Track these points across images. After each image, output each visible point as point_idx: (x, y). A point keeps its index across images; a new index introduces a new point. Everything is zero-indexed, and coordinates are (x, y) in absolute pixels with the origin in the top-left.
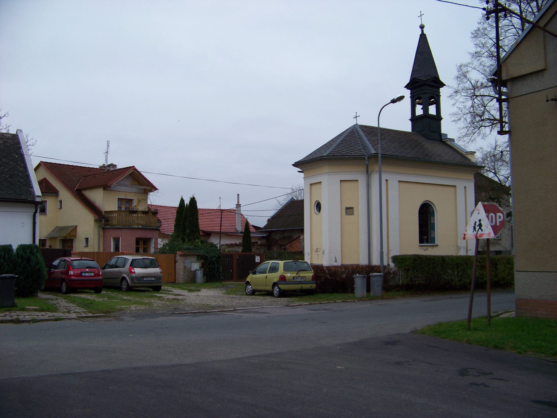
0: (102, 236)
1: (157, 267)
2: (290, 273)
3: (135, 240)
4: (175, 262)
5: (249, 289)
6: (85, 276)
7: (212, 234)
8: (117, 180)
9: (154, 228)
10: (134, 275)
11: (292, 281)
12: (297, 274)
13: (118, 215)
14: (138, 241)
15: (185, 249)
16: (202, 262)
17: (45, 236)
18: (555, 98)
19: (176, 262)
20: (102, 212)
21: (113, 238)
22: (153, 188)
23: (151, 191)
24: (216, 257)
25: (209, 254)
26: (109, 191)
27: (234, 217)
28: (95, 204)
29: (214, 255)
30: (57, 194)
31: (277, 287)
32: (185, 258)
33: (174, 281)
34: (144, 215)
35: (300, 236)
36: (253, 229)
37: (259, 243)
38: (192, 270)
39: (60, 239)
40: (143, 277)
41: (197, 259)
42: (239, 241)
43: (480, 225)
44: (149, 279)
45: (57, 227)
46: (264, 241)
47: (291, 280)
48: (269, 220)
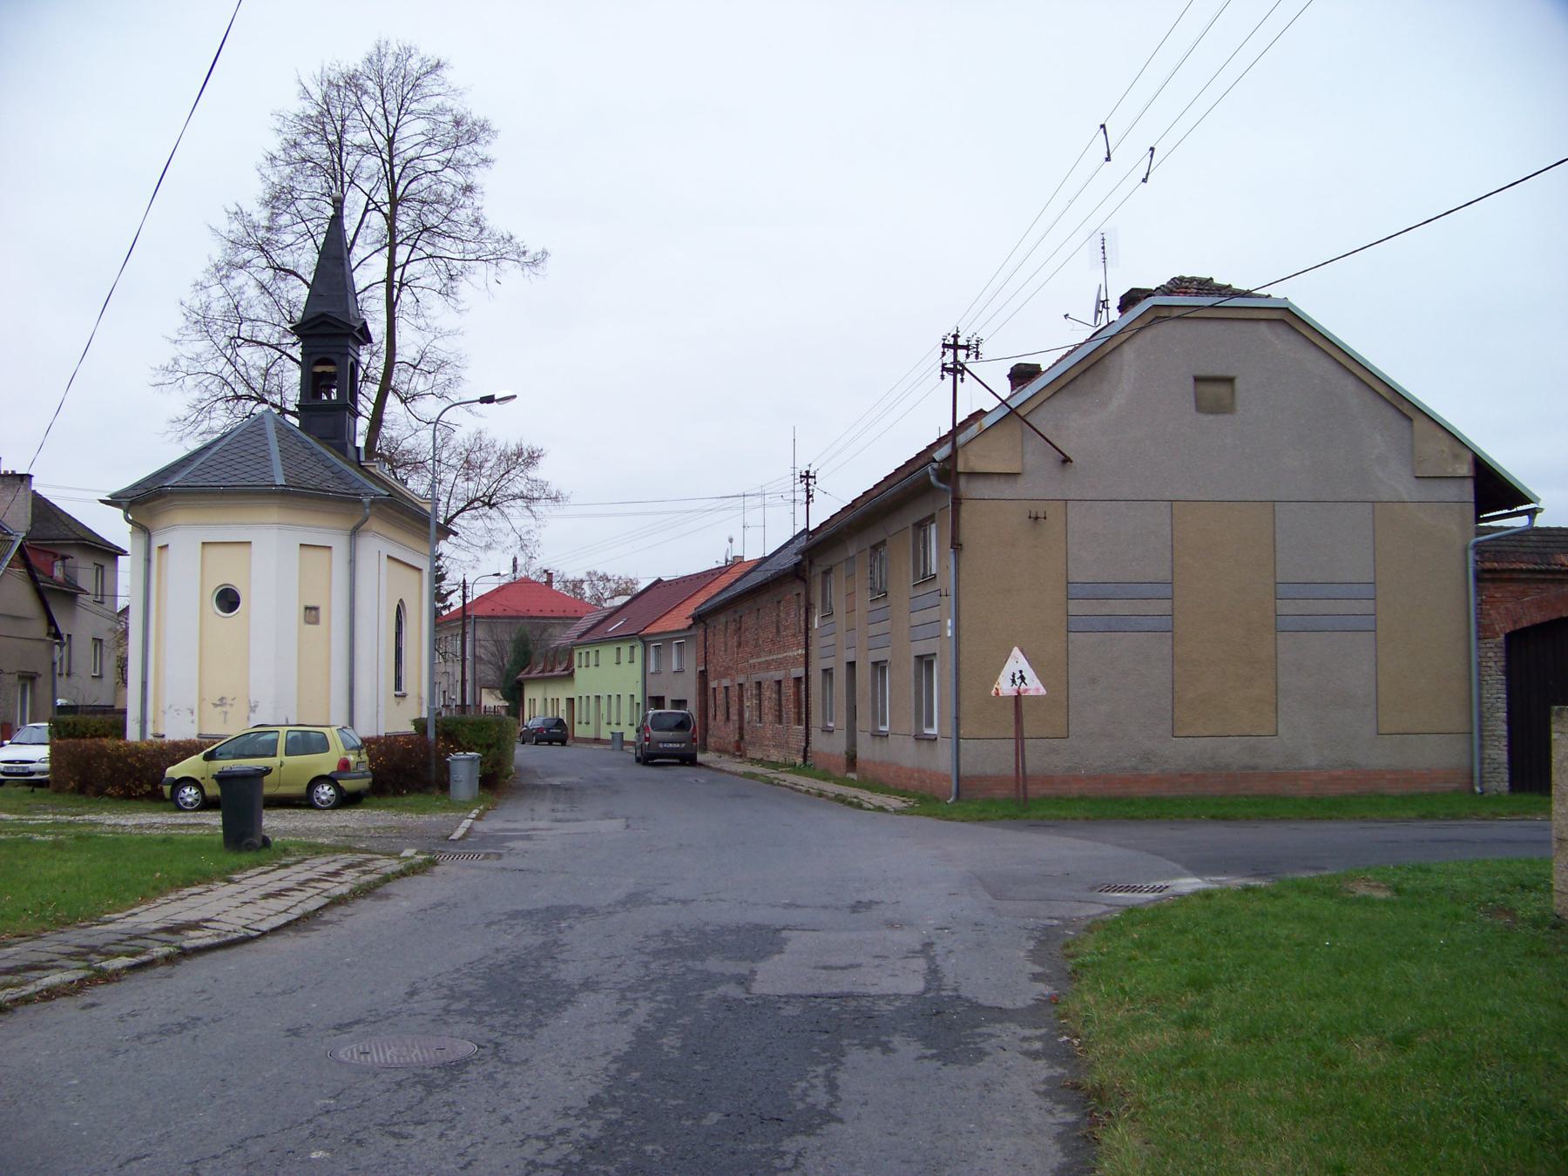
18: (972, 475)
43: (1022, 678)
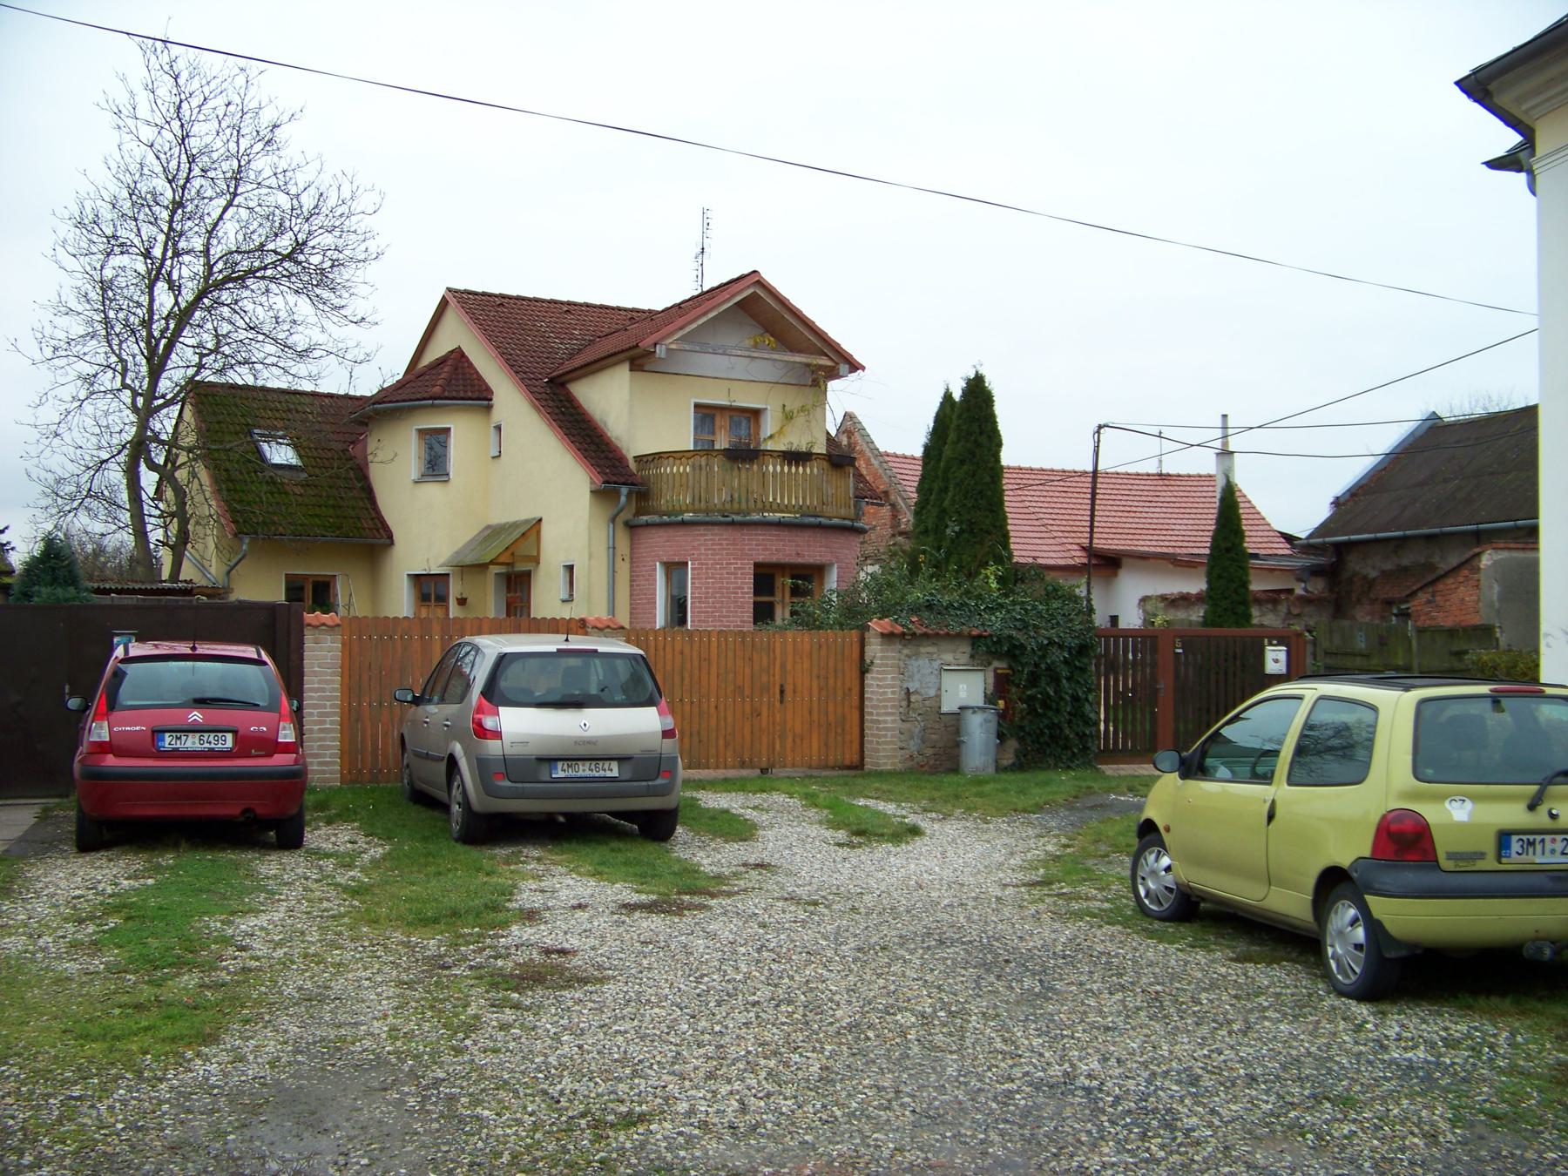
0: (627, 559)
1: (650, 702)
2: (1474, 798)
3: (750, 570)
4: (863, 670)
5: (1154, 873)
6: (176, 750)
7: (1125, 561)
8: (681, 328)
9: (835, 521)
10: (493, 747)
11: (1490, 863)
12: (1532, 807)
13: (693, 467)
14: (765, 577)
15: (915, 609)
16: (996, 669)
17: (442, 560)
19: (867, 671)
20: (627, 459)
21: (661, 563)
22: (840, 362)
23: (833, 374)
24: (1070, 649)
25: (1032, 634)
26: (648, 374)
27: (1210, 500)
28: (606, 431)
29: (1056, 640)
30: (486, 402)
31: (1352, 912)
32: (906, 651)
33: (856, 758)
34: (797, 467)
35: (1478, 555)
36: (1281, 545)
37: (1299, 591)
38: (945, 709)
39: (496, 574)
40: (551, 760)
41: (972, 657)
42: (1195, 585)
44: (584, 770)
45: (489, 527)
46: (1318, 586)
47: (1481, 855)
48: (1337, 503)
